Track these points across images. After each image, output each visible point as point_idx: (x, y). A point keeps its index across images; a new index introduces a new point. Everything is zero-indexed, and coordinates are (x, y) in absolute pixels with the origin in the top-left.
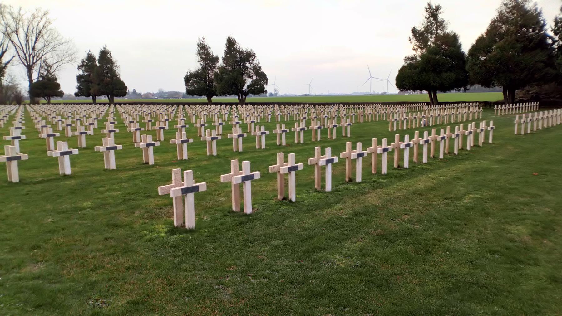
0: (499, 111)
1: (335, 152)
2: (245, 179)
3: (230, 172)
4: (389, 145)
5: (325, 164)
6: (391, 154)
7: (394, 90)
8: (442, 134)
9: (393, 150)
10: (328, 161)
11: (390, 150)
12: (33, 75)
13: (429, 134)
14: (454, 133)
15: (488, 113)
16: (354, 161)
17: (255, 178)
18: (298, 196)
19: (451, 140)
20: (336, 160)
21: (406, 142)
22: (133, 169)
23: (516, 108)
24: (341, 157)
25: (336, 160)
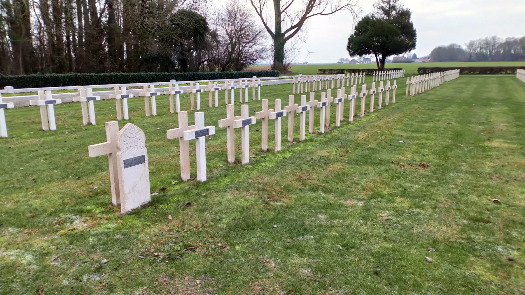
0: (360, 79)
1: (210, 120)
2: (198, 134)
3: (178, 127)
4: (282, 108)
5: (194, 138)
6: (256, 128)
7: (346, 55)
8: (324, 99)
9: (259, 122)
10: (245, 123)
11: (254, 122)
12: (271, 30)
13: (308, 99)
14: (320, 100)
15: (369, 78)
16: (238, 131)
17: (210, 134)
18: (209, 175)
19: (333, 105)
20: (212, 130)
21: (279, 109)
22: (470, 60)
23: (378, 76)
24: (221, 126)
25: (212, 130)
